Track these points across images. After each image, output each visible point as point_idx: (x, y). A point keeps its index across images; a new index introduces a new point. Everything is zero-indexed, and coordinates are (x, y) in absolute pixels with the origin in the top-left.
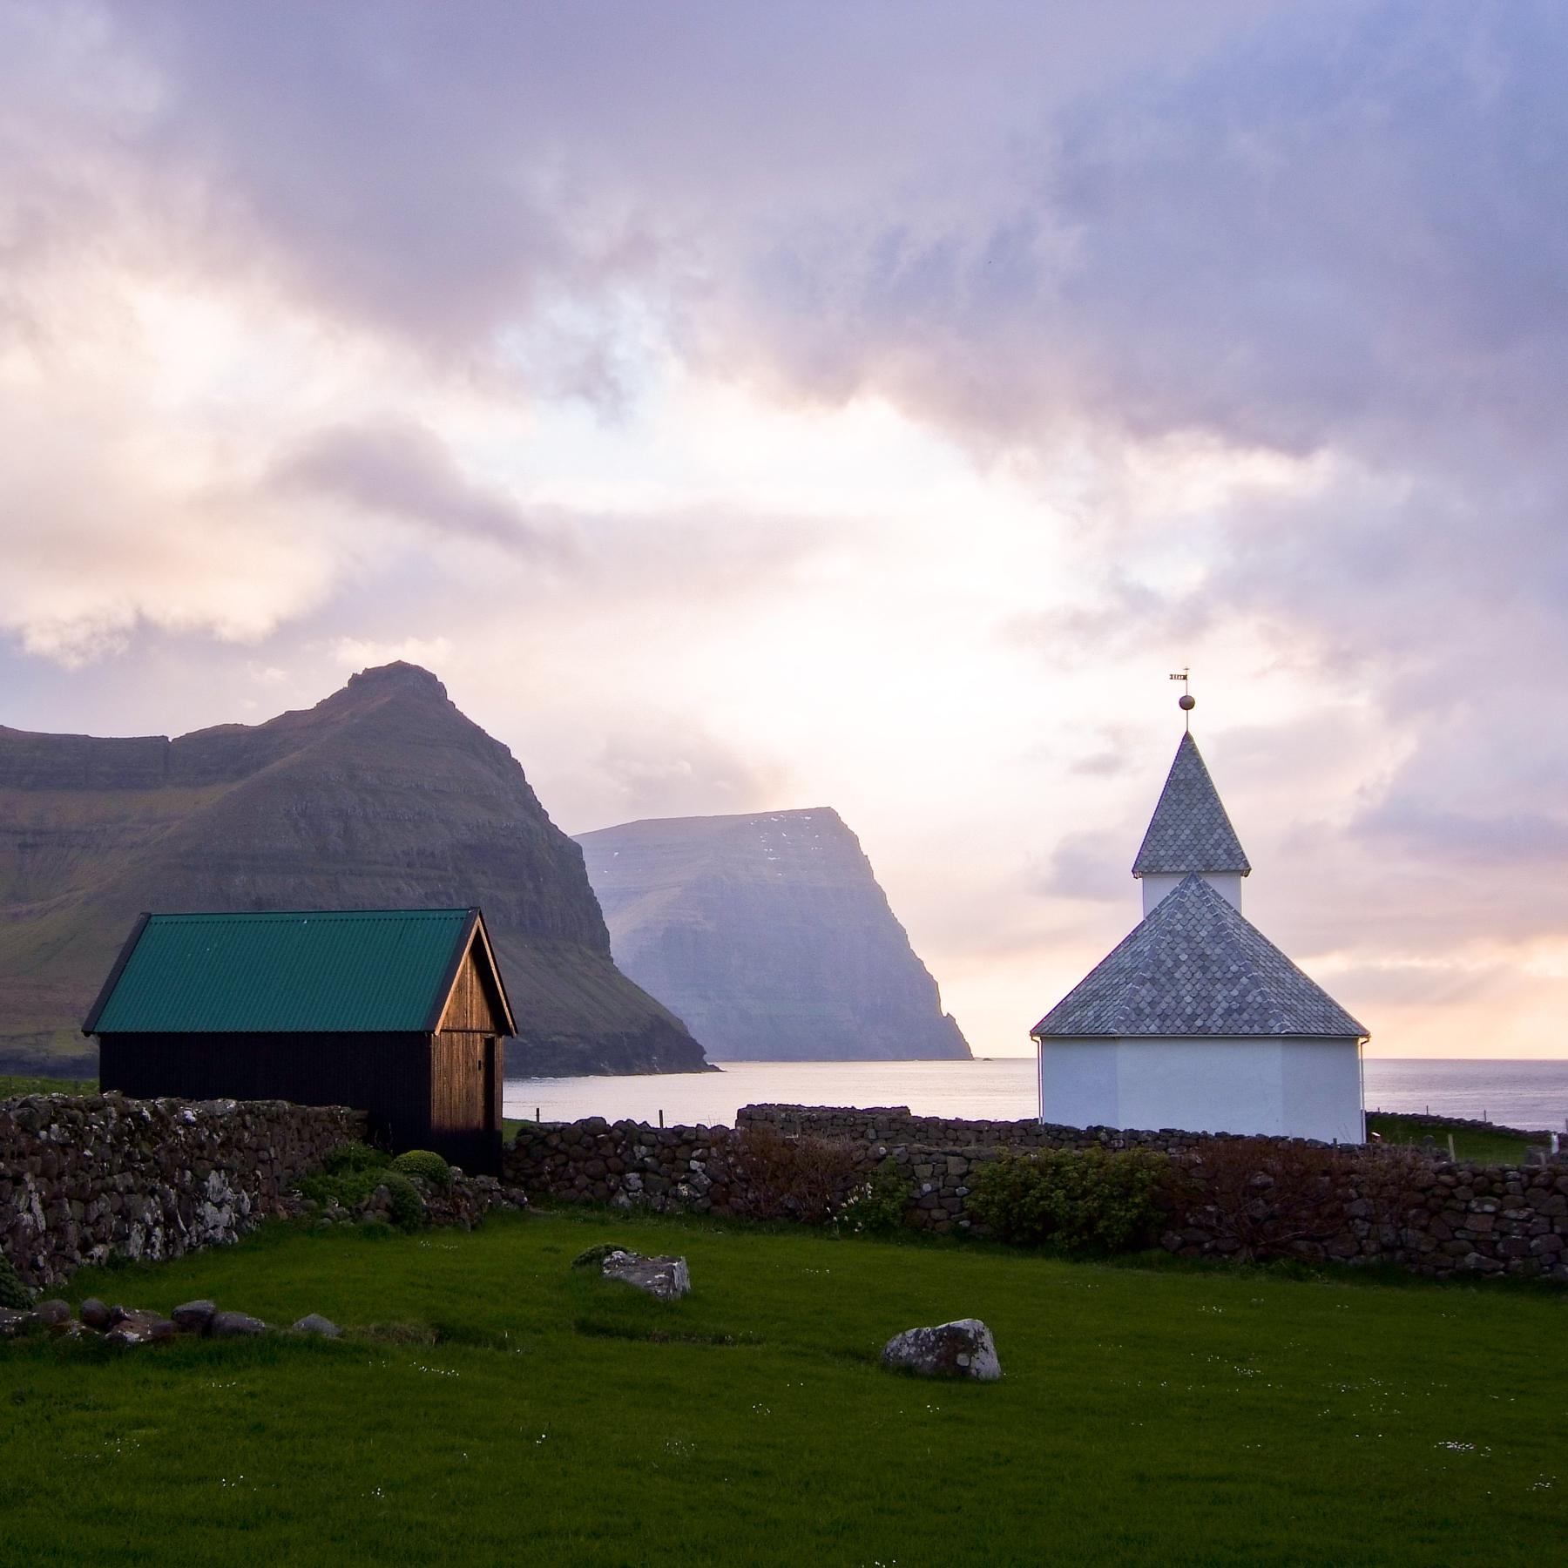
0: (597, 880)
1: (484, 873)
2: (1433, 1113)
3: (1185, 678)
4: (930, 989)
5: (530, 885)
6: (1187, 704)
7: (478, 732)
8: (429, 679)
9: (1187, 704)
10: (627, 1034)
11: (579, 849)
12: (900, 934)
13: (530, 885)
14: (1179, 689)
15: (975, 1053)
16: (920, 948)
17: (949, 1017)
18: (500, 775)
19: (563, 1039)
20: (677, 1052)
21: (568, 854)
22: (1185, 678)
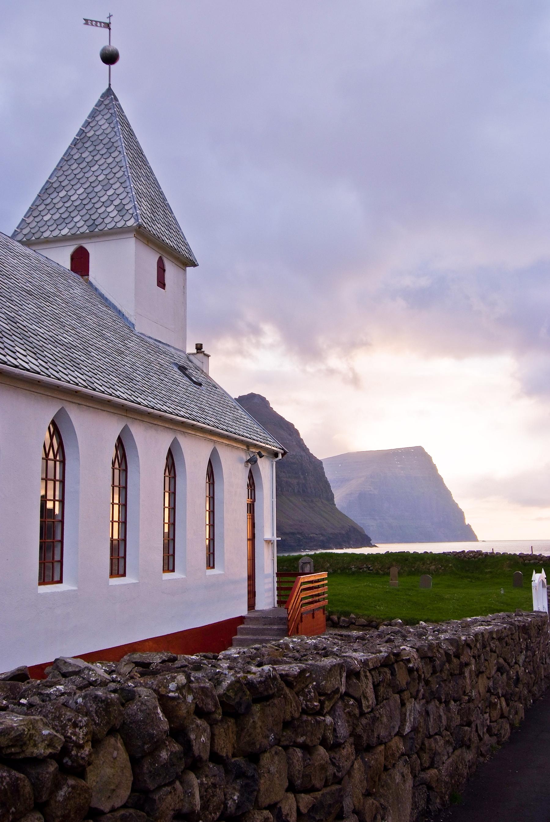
0: (329, 475)
1: (284, 472)
2: (537, 553)
3: (108, 26)
4: (461, 514)
5: (302, 477)
6: (110, 58)
7: (282, 419)
8: (263, 399)
9: (110, 58)
10: (340, 534)
11: (321, 463)
12: (447, 494)
13: (302, 477)
14: (100, 40)
15: (479, 538)
16: (456, 498)
17: (469, 526)
18: (290, 435)
19: (314, 535)
20: (366, 542)
21: (317, 465)
22: (108, 26)
